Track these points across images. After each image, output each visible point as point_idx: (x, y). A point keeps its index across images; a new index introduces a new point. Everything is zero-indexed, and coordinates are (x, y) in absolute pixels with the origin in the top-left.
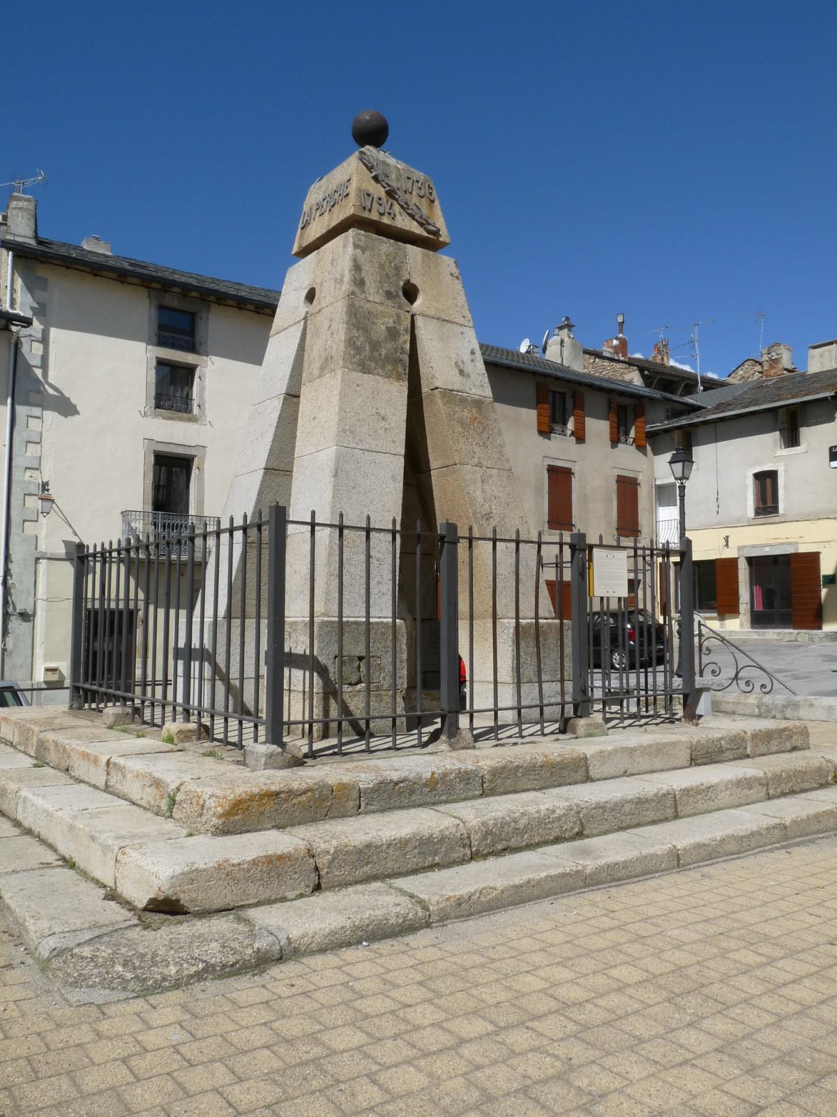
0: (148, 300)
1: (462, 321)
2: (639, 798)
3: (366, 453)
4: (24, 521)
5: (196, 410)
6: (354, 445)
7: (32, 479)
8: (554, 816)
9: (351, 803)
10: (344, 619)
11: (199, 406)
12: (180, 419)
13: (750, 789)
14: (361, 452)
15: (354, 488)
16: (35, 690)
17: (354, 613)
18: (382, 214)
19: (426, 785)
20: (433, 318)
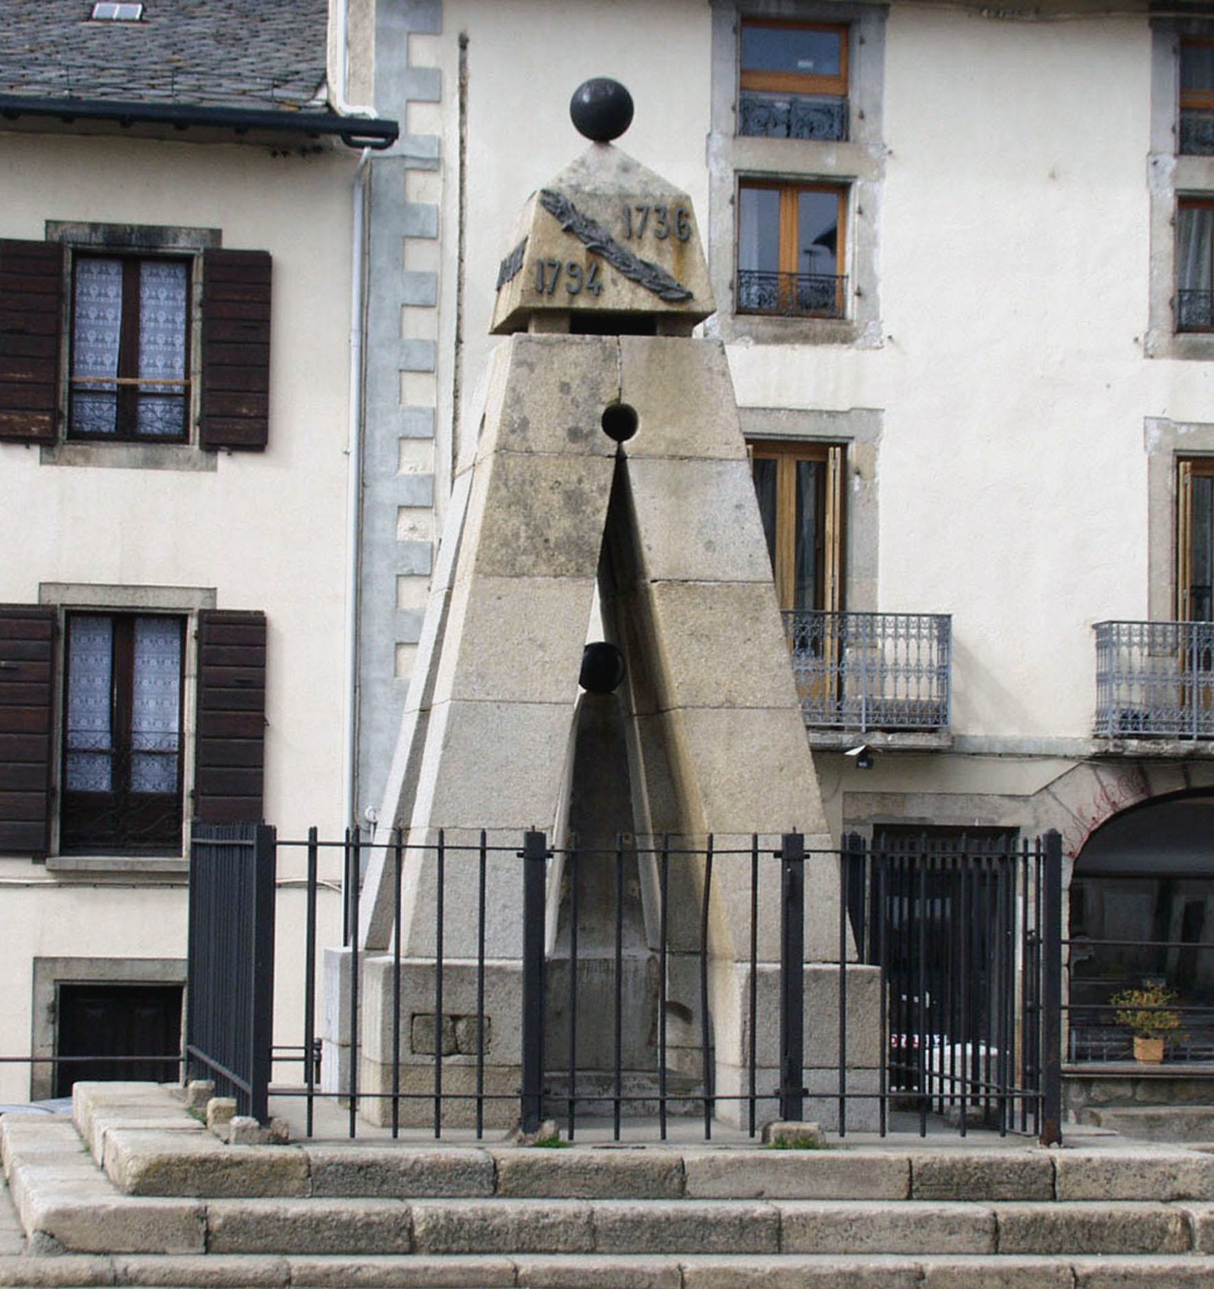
0: (710, 11)
1: (721, 452)
2: (705, 1218)
3: (503, 706)
4: (399, 645)
5: (852, 307)
6: (483, 696)
7: (415, 537)
8: (546, 1221)
9: (296, 1182)
10: (445, 961)
11: (859, 294)
12: (807, 339)
13: (950, 1234)
14: (495, 705)
15: (475, 764)
16: (842, 1102)
17: (461, 955)
18: (574, 294)
19: (404, 1174)
20: (661, 457)
